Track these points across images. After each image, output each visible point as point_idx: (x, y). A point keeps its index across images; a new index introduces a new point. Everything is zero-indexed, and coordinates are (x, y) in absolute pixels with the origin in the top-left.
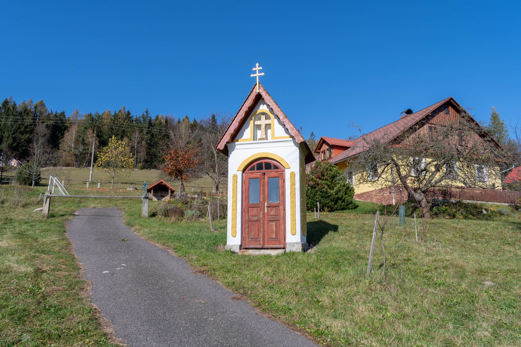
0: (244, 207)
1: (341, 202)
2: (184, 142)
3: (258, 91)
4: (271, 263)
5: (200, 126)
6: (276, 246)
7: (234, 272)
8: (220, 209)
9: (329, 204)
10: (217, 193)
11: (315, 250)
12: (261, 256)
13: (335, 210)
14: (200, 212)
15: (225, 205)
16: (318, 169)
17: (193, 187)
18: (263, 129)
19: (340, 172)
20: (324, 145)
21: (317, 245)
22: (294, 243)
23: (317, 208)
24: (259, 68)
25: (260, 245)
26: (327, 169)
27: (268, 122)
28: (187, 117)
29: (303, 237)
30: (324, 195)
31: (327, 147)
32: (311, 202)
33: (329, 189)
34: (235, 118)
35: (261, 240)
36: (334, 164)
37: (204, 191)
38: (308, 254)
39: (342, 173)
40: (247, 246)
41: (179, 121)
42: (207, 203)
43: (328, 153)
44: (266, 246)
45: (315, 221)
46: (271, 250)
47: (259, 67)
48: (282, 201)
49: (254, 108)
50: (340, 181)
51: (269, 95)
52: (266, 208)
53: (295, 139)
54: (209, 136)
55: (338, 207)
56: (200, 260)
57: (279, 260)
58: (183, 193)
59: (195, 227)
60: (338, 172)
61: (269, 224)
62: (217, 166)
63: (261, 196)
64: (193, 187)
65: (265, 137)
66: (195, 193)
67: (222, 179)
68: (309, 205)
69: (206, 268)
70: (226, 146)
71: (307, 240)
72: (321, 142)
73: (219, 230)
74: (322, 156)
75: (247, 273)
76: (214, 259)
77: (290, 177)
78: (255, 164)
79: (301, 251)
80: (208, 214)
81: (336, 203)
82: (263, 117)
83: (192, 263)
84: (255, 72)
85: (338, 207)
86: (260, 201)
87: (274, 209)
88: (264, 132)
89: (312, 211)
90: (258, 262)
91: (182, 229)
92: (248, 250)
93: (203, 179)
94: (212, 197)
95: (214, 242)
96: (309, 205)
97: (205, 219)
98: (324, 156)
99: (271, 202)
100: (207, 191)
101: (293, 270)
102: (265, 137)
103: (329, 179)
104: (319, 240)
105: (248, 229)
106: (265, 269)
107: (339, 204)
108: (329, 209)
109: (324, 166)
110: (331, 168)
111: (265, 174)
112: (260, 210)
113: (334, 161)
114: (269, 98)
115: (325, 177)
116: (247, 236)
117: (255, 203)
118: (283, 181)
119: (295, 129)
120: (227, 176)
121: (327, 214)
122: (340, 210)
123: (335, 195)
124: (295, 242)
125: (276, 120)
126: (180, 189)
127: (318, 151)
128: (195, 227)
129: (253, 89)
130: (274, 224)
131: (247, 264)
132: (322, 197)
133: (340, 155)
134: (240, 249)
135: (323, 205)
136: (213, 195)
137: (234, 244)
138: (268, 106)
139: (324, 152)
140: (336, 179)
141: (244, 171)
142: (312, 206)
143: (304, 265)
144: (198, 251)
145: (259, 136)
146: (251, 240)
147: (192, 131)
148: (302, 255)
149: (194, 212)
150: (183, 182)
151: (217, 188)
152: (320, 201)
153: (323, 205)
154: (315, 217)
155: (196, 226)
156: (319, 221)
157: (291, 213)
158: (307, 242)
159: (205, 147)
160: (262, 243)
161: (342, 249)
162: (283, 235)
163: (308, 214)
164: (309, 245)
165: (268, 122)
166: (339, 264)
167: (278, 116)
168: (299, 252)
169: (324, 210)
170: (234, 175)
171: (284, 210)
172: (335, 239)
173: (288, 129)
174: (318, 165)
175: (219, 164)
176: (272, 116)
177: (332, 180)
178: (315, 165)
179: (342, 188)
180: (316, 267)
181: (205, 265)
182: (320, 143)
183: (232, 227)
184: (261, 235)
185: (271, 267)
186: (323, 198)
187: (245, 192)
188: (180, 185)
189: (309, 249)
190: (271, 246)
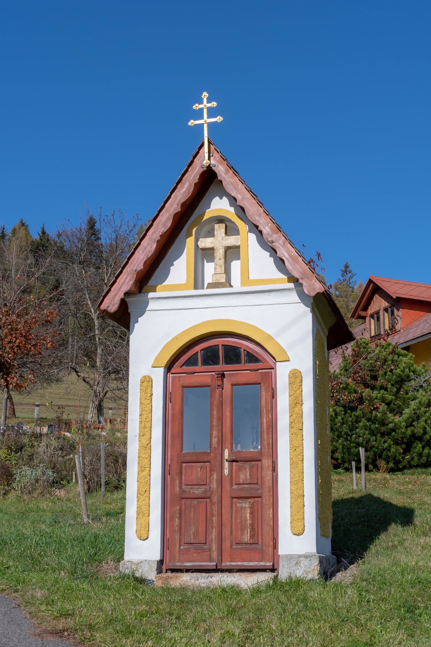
0: (169, 462)
1: (420, 445)
2: (16, 288)
3: (206, 162)
4: (240, 608)
5: (56, 248)
6: (251, 564)
7: (144, 634)
8: (107, 465)
9: (389, 451)
10: (100, 422)
11: (354, 575)
12: (214, 591)
13: (405, 467)
14: (54, 472)
15: (121, 454)
16: (362, 361)
17: (38, 406)
18: (220, 259)
19: (419, 368)
20: (377, 298)
21: (360, 562)
22: (300, 556)
23: (358, 461)
24: (209, 105)
25: (210, 561)
26: (385, 360)
27: (232, 241)
28: (23, 224)
29: (324, 539)
30: (377, 428)
31: (385, 304)
32: (343, 446)
33: (391, 412)
34: (147, 231)
35: (214, 547)
36: (404, 349)
37: (65, 417)
38: (336, 585)
39: (423, 371)
40: (178, 565)
41: (3, 232)
42: (72, 447)
43: (386, 319)
44: (227, 564)
45: (353, 498)
46: (238, 574)
47: (209, 101)
48: (268, 445)
49: (196, 207)
50: (418, 390)
51: (236, 172)
52: (226, 464)
53: (301, 285)
54: (81, 273)
55: (412, 459)
56: (53, 601)
57: (258, 601)
58: (12, 422)
59: (41, 513)
60: (412, 369)
61: (234, 505)
62: (99, 351)
63: (215, 433)
64: (38, 406)
65: (224, 281)
66: (41, 421)
67: (113, 384)
68: (338, 455)
69: (70, 622)
70: (123, 304)
71: (333, 548)
72: (369, 291)
73: (104, 519)
74: (373, 327)
75: (176, 635)
76: (90, 598)
77: (290, 384)
78: (198, 348)
79: (317, 577)
80: (76, 478)
81: (407, 450)
82: (220, 229)
83: (33, 609)
84: (199, 115)
85: (412, 459)
86: (211, 446)
87: (247, 466)
88: (223, 269)
89: (348, 470)
90: (205, 608)
91: (6, 517)
92: (179, 574)
93: (63, 386)
94: (87, 434)
95: (92, 551)
96: (338, 455)
97: (68, 492)
98: (378, 326)
99: (239, 448)
100: (73, 417)
101: (296, 628)
102: (224, 281)
103: (389, 386)
104: (365, 548)
105: (180, 518)
106: (224, 626)
107: (417, 450)
108: (391, 465)
109: (377, 351)
110: (396, 357)
111: (223, 376)
112: (211, 471)
113: (402, 340)
114: (236, 179)
115: (381, 381)
116: (177, 537)
117: (198, 450)
118: (270, 394)
119: (300, 259)
120: (125, 378)
121: (385, 479)
122: (417, 466)
123: (407, 427)
124: (303, 553)
125: (252, 237)
126: (4, 410)
127: (363, 313)
128: (41, 513)
129: (195, 157)
130: (247, 505)
131: (176, 613)
132: (372, 433)
133: (417, 323)
134: (159, 571)
135: (375, 453)
136: (89, 428)
137: (143, 558)
138: (233, 200)
139: (375, 316)
140: (408, 386)
141: (169, 367)
142: (346, 456)
143: (326, 614)
144: (51, 576)
145: (208, 279)
146: (186, 547)
147: (37, 260)
148: (319, 589)
149: (39, 472)
150: (12, 393)
151: (100, 409)
152: (367, 442)
153: (375, 453)
154: (355, 487)
155: (44, 511)
156: (365, 496)
157: (291, 478)
158: (333, 554)
159: (69, 301)
160: (215, 555)
161: (423, 572)
162: (271, 536)
163: (334, 477)
164: (339, 561)
165: (232, 241)
166: (417, 612)
167: (257, 227)
168: (312, 580)
169: (377, 468)
170: (145, 377)
171: (274, 469)
172: (406, 544)
173: (283, 261)
174: (362, 350)
175: (106, 346)
176: (242, 226)
177: (398, 390)
178: (353, 350)
179: (423, 409)
180: (357, 619)
181: (67, 615)
182: (367, 294)
183: (138, 513)
184: (214, 534)
185: (240, 620)
186: (376, 435)
187: (172, 422)
188: (4, 401)
189: (339, 571)
190: (239, 563)
